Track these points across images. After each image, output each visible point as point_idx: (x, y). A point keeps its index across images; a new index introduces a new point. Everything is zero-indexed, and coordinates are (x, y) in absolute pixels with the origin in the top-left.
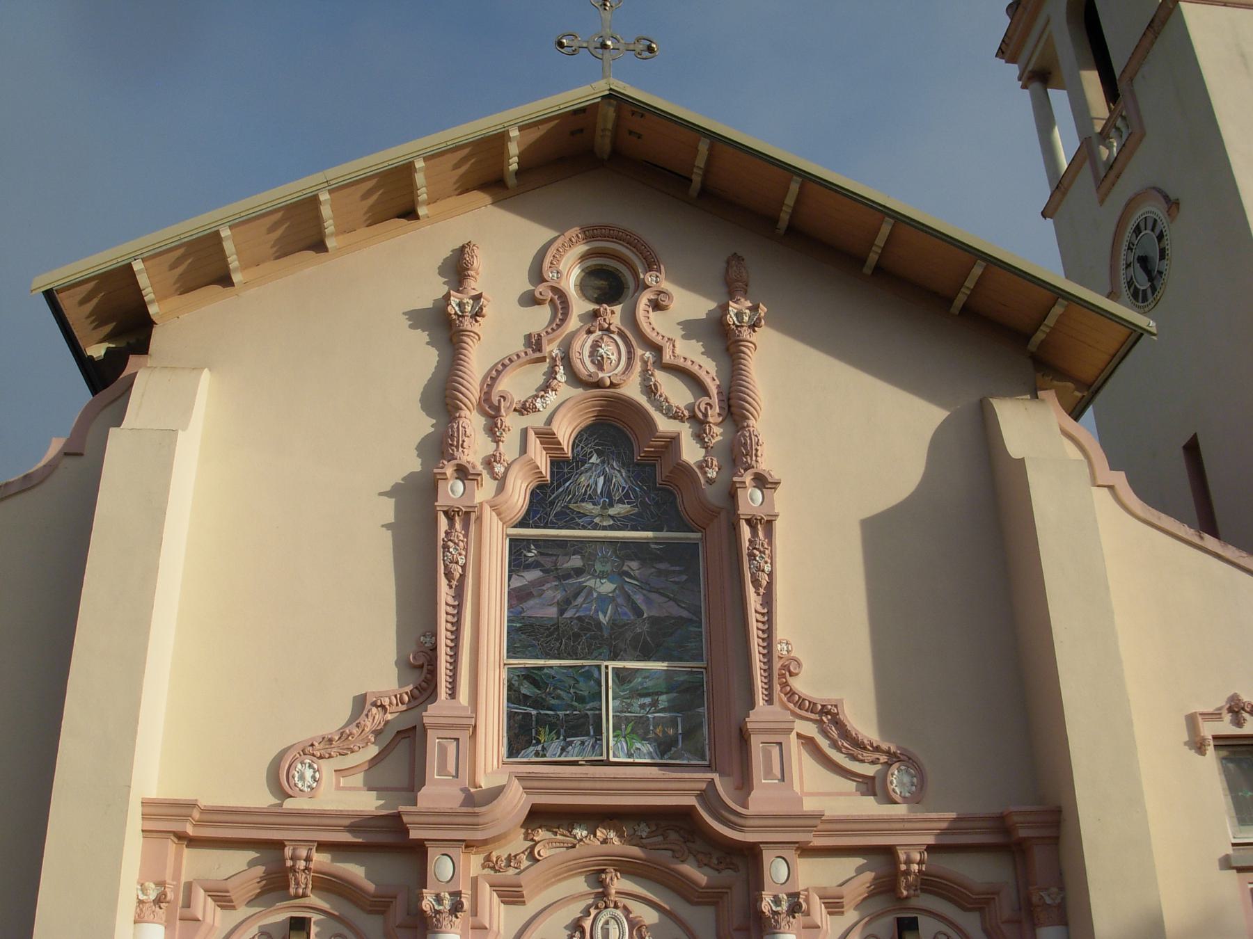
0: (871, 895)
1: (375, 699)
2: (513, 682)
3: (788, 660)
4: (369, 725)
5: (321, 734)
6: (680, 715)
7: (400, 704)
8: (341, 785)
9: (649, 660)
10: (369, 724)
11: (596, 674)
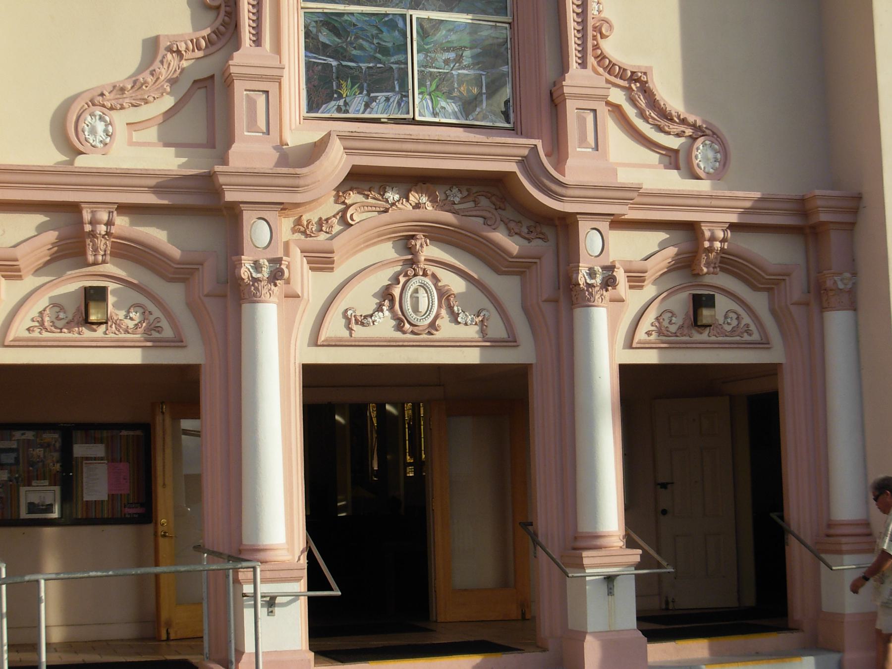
0: (671, 270)
1: (169, 44)
2: (310, 28)
3: (599, 21)
4: (164, 73)
5: (113, 81)
6: (485, 73)
7: (196, 50)
8: (134, 140)
9: (451, 10)
10: (163, 71)
11: (400, 24)
